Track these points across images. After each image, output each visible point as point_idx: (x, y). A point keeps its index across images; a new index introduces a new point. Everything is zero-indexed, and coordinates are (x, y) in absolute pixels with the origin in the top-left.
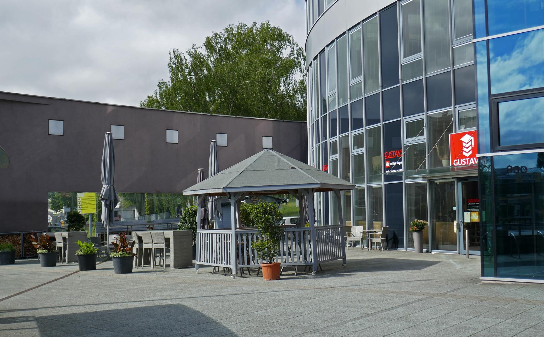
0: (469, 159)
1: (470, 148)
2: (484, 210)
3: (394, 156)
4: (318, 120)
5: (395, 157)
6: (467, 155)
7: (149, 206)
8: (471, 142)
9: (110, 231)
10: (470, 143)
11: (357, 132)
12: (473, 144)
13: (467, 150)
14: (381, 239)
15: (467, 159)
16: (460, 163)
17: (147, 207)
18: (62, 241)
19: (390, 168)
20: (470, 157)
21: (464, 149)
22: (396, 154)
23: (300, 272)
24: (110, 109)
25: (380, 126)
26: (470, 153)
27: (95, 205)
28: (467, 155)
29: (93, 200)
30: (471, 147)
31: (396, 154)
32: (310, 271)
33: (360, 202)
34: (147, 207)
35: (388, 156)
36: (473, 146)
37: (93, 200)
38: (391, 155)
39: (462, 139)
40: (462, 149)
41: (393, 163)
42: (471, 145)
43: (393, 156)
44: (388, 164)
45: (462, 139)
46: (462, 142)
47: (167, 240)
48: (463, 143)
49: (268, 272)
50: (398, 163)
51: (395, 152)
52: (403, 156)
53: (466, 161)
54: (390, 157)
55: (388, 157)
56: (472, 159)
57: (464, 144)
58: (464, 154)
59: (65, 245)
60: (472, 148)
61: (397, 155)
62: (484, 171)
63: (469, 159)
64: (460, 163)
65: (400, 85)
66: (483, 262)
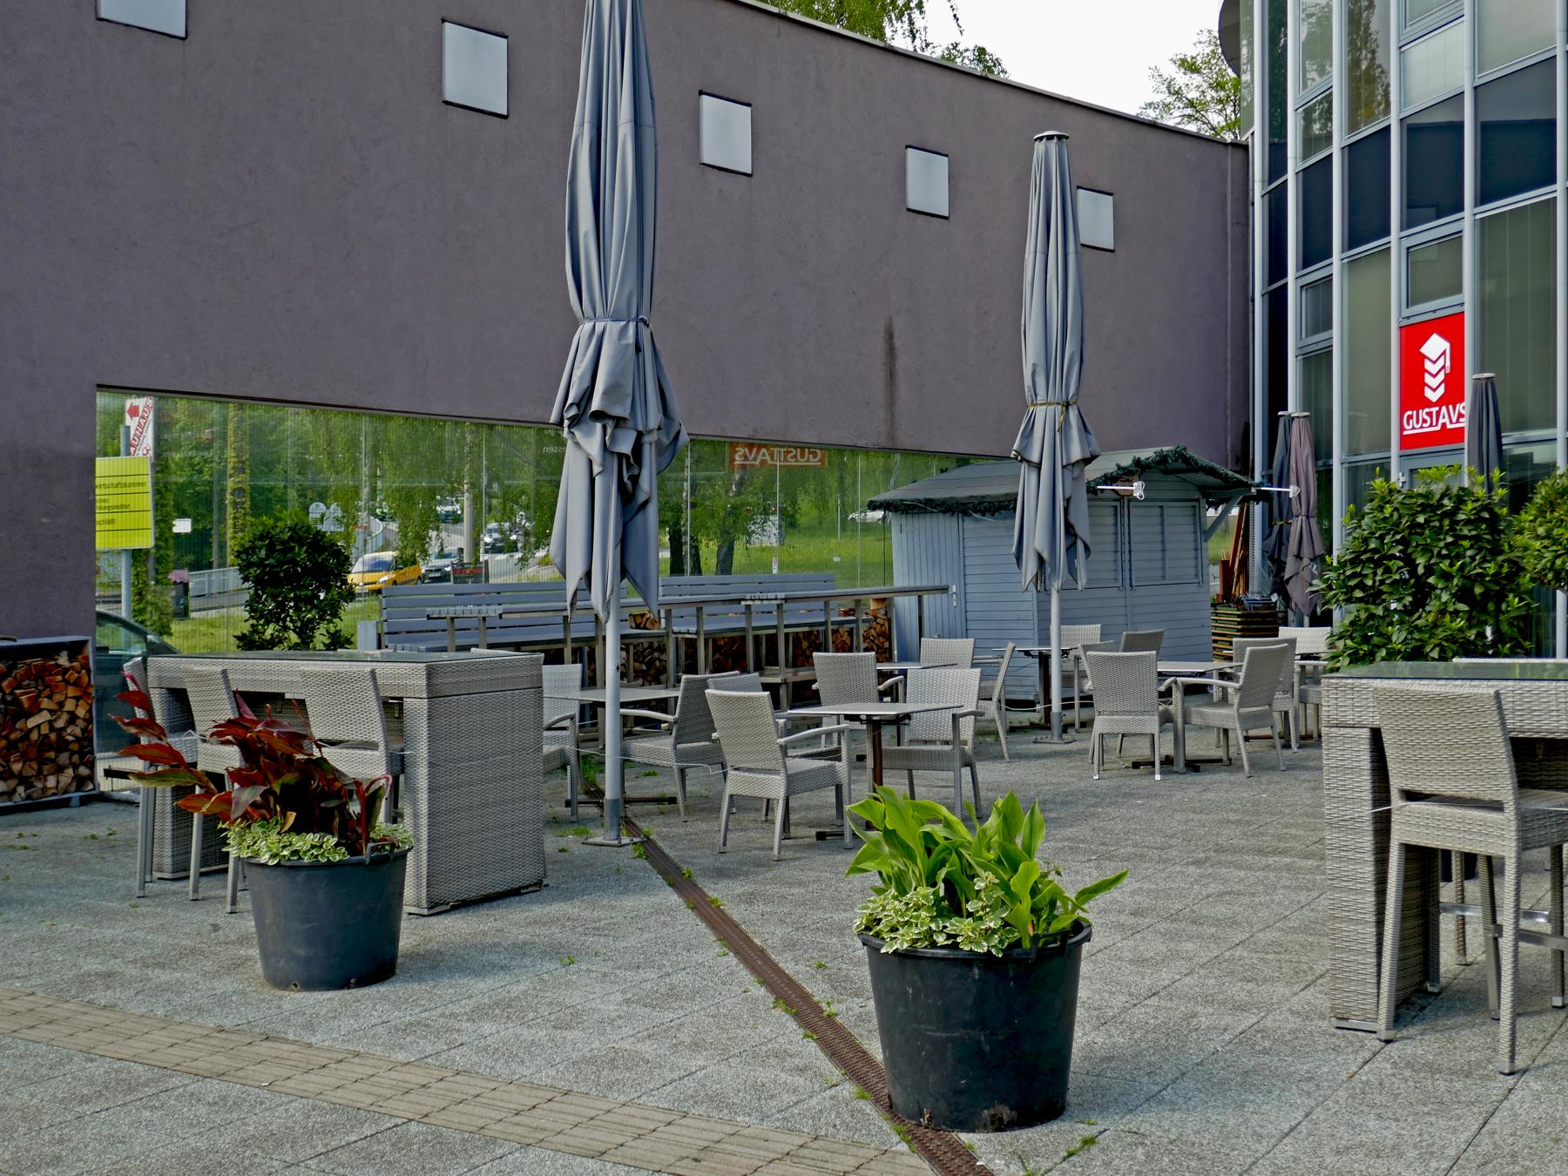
0: (1437, 409)
1: (1441, 376)
2: (195, 522)
3: (1437, 425)
5: (1438, 428)
7: (241, 534)
8: (1443, 358)
10: (1440, 363)
12: (1448, 364)
14: (1239, 714)
15: (1434, 410)
16: (1418, 422)
17: (234, 537)
18: (378, 736)
20: (1440, 403)
21: (1428, 379)
22: (1444, 417)
24: (1490, 286)
26: (1441, 390)
27: (150, 495)
29: (140, 489)
30: (1443, 371)
31: (1444, 417)
34: (234, 537)
35: (1416, 426)
36: (1448, 371)
37: (140, 489)
38: (1425, 421)
40: (1423, 378)
42: (1444, 367)
43: (1431, 425)
46: (1425, 357)
48: (1427, 362)
51: (1438, 413)
53: (1430, 414)
54: (1421, 427)
55: (1413, 428)
56: (1444, 408)
57: (1428, 365)
59: (399, 765)
60: (1446, 375)
61: (1446, 420)
62: (438, 508)
63: (1437, 409)
64: (1418, 422)
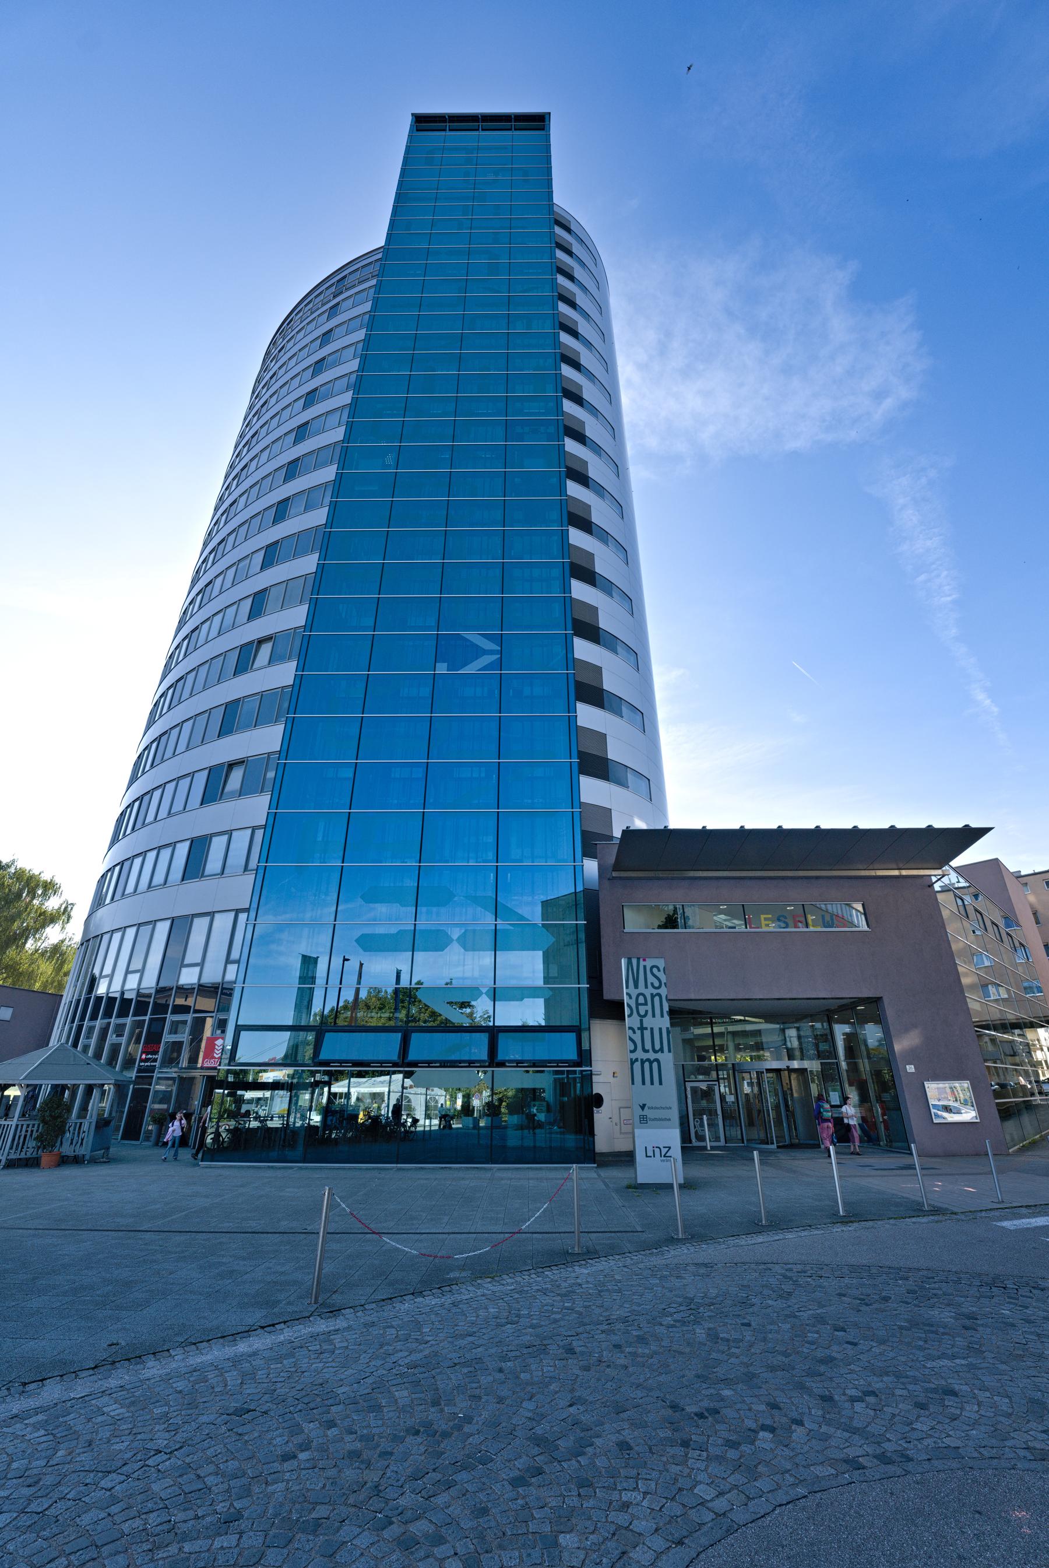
4: (72, 1002)
6: (217, 1056)
9: (799, 1057)
11: (121, 1021)
13: (218, 1052)
19: (147, 1060)
23: (808, 675)
25: (145, 1020)
28: (217, 1056)
32: (293, 1146)
33: (147, 1060)
39: (216, 1042)
41: (150, 1056)
44: (144, 1056)
45: (216, 1042)
47: (823, 1144)
49: (658, 879)
50: (154, 1056)
52: (161, 1050)
57: (216, 1047)
58: (215, 1055)
65: (147, 1018)
66: (548, 965)
